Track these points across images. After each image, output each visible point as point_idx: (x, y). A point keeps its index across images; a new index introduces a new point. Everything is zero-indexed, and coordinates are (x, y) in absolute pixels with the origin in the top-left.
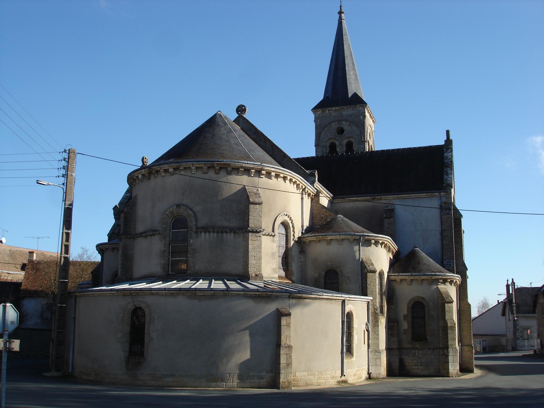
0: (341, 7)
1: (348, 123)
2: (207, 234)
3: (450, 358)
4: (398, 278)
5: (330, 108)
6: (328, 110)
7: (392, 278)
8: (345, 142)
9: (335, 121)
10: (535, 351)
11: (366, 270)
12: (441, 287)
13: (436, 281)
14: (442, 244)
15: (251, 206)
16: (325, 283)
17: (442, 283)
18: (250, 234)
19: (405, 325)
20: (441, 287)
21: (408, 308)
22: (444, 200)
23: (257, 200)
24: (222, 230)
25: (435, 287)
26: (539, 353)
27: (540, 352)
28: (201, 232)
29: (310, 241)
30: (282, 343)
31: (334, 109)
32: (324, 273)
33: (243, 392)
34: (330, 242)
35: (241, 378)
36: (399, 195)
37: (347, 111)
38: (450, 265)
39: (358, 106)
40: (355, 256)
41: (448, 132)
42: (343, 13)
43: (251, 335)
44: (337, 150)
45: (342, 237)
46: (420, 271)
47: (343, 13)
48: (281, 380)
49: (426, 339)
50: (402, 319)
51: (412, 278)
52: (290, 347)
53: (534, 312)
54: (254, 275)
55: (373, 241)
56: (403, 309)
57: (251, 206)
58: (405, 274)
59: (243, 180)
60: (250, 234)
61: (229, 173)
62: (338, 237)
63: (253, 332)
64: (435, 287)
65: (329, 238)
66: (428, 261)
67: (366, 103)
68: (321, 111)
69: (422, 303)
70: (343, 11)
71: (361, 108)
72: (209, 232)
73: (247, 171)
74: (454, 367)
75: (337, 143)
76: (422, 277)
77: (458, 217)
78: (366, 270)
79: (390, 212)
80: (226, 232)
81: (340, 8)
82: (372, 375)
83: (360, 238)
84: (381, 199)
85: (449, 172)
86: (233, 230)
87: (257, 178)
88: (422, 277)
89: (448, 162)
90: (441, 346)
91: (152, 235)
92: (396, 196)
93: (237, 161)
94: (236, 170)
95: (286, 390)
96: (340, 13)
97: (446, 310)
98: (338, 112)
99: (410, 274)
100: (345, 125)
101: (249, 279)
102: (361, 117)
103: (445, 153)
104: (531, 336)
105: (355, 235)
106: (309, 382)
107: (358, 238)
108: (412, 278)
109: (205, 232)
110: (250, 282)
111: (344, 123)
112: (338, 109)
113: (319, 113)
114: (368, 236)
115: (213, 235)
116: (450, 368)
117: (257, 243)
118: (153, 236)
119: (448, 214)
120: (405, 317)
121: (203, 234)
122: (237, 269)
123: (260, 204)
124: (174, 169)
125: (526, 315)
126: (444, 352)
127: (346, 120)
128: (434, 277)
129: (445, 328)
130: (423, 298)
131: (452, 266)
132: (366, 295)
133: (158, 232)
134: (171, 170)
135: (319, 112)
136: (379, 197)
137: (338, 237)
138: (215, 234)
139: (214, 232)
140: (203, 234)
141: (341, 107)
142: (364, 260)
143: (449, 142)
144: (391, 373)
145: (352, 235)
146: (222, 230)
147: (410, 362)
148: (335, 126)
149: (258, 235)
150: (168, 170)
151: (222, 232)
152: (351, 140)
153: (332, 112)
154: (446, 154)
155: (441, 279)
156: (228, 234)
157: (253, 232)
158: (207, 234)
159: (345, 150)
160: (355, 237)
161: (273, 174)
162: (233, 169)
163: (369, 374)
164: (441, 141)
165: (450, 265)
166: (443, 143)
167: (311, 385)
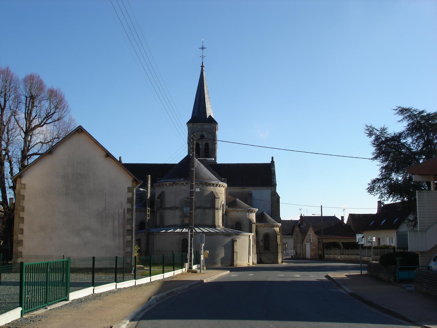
0: (202, 63)
1: (207, 133)
2: (199, 209)
3: (279, 257)
4: (259, 225)
5: (197, 124)
6: (196, 124)
7: (257, 225)
8: (204, 143)
9: (200, 131)
10: (292, 256)
11: (252, 223)
12: (275, 228)
13: (274, 226)
14: (272, 210)
15: (216, 199)
16: (236, 228)
17: (275, 227)
18: (216, 210)
19: (261, 244)
20: (275, 228)
21: (263, 237)
22: (273, 190)
23: (218, 197)
24: (205, 208)
25: (273, 229)
26: (294, 257)
27: (295, 257)
28: (197, 209)
29: (229, 211)
30: (235, 251)
31: (199, 124)
32: (235, 224)
33: (63, 293)
34: (238, 211)
35: (222, 263)
36: (254, 187)
37: (207, 126)
38: (275, 218)
39: (213, 124)
40: (247, 217)
41: (272, 158)
42: (204, 67)
43: (225, 248)
44: (199, 147)
45: (243, 210)
46: (267, 222)
47: (204, 67)
48: (234, 264)
49: (270, 249)
50: (260, 241)
51: (265, 225)
52: (237, 252)
53: (292, 235)
54: (217, 226)
55: (253, 211)
56: (261, 238)
57: (216, 199)
58: (263, 223)
59: (211, 189)
60: (216, 210)
61: (207, 186)
62: (241, 210)
63: (225, 247)
64: (273, 229)
65: (238, 210)
66: (270, 218)
67: (217, 123)
68: (192, 125)
69: (268, 235)
70: (204, 66)
71: (214, 125)
72: (200, 209)
73: (213, 185)
74: (280, 260)
75: (200, 143)
76: (269, 225)
77: (278, 198)
78: (252, 223)
79: (250, 195)
80: (206, 209)
81: (202, 63)
82: (254, 263)
83: (250, 210)
84: (246, 189)
85: (274, 177)
86: (209, 208)
87: (216, 187)
88: (269, 225)
89: (273, 173)
90: (275, 252)
91: (175, 209)
92: (253, 188)
93: (210, 181)
94: (210, 185)
95: (236, 267)
96: (202, 67)
97: (277, 238)
98: (201, 126)
99: (264, 224)
100: (205, 134)
101: (216, 227)
102: (214, 130)
103: (272, 167)
104: (288, 248)
105: (248, 209)
106: (241, 264)
107: (249, 210)
108: (265, 225)
109: (199, 209)
110: (217, 228)
111: (204, 132)
112: (201, 124)
113: (190, 125)
114: (252, 209)
115: (202, 210)
116: (279, 260)
117: (218, 213)
118: (176, 210)
119: (275, 197)
120: (262, 241)
121: (198, 209)
122: (210, 222)
123: (219, 198)
124: (186, 183)
125: (285, 236)
126: (276, 254)
127: (206, 131)
128: (273, 225)
129: (277, 245)
130: (269, 233)
131: (276, 219)
132: (252, 233)
133: (179, 208)
134: (185, 184)
135: (191, 125)
136: (245, 188)
137: (241, 210)
138: (202, 210)
139: (202, 209)
140: (198, 209)
141: (203, 124)
142: (251, 219)
143: (273, 162)
144: (258, 263)
145: (247, 209)
146: (205, 208)
147: (263, 258)
148: (199, 134)
149: (218, 210)
150: (183, 183)
151: (205, 209)
152: (208, 142)
153: (198, 126)
154: (272, 168)
155: (275, 225)
156: (207, 210)
157: (217, 209)
158: (199, 209)
159: (204, 147)
160: (247, 210)
161: (221, 185)
162: (209, 184)
163: (253, 263)
164: (269, 161)
165: (275, 218)
166: (270, 162)
167: (241, 266)
